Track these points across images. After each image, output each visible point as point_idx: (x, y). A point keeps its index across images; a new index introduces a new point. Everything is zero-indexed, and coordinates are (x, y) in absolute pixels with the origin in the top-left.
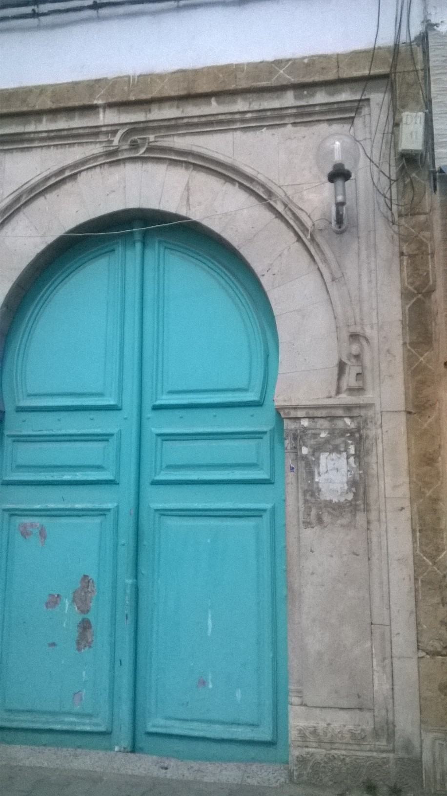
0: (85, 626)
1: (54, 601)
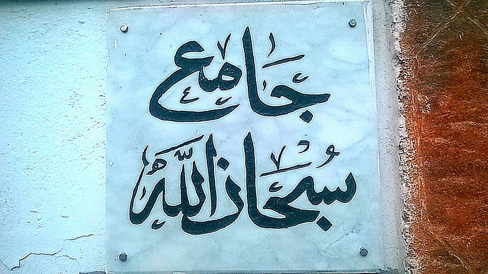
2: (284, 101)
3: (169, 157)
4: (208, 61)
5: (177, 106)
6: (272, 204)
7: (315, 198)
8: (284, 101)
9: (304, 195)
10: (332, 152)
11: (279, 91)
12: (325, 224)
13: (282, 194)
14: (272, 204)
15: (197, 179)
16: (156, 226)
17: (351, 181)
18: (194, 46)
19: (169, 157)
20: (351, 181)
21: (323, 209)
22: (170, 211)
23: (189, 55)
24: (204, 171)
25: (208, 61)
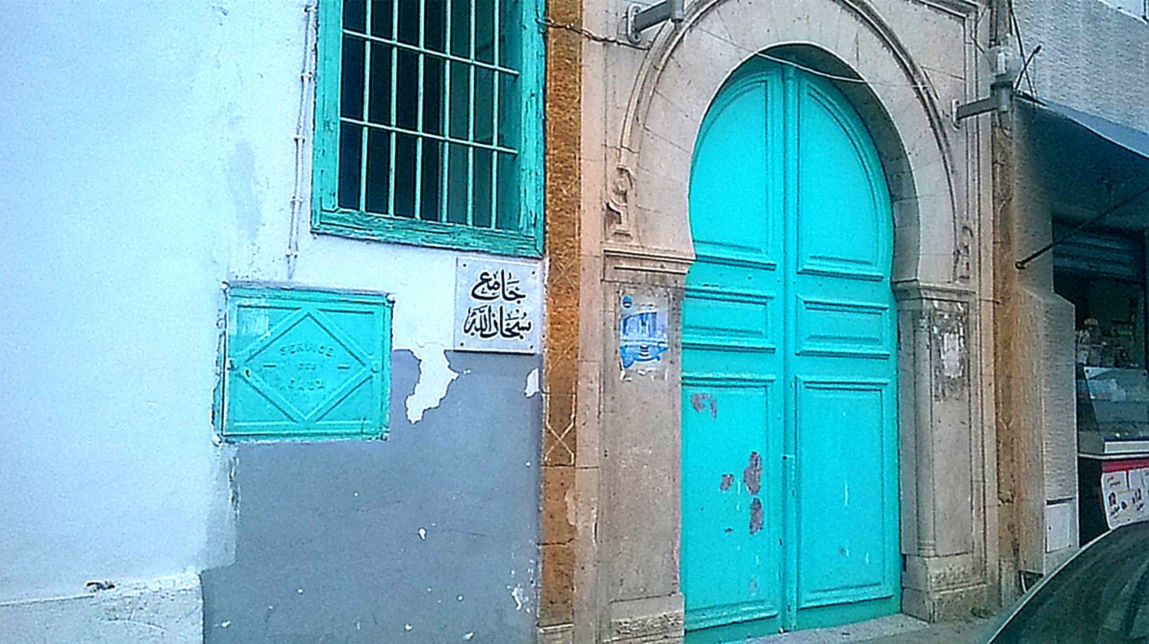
0: (756, 506)
1: (727, 482)
2: (513, 296)
3: (477, 312)
4: (490, 279)
5: (481, 295)
6: (507, 330)
7: (519, 329)
8: (513, 296)
9: (516, 328)
10: (525, 314)
11: (511, 293)
12: (522, 337)
13: (510, 327)
14: (507, 330)
15: (485, 320)
16: (473, 334)
17: (530, 324)
18: (486, 274)
19: (477, 312)
20: (530, 324)
21: (521, 332)
22: (477, 330)
23: (485, 277)
24: (498, 322)
25: (490, 279)
